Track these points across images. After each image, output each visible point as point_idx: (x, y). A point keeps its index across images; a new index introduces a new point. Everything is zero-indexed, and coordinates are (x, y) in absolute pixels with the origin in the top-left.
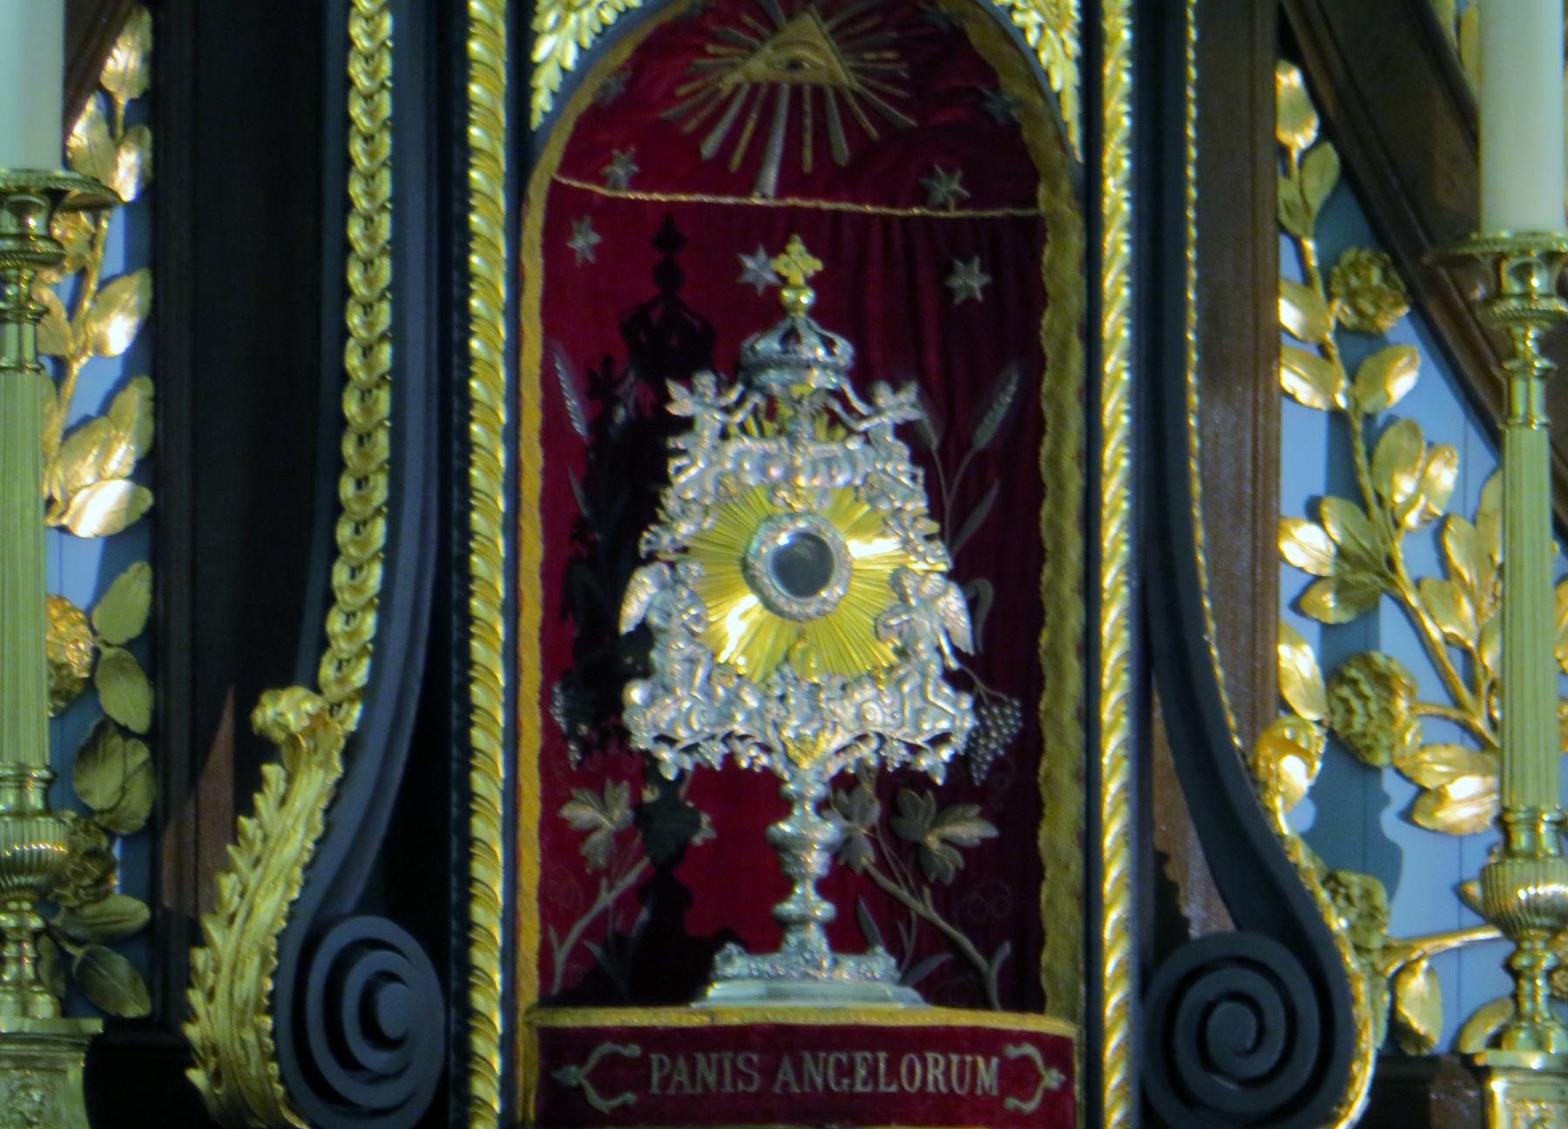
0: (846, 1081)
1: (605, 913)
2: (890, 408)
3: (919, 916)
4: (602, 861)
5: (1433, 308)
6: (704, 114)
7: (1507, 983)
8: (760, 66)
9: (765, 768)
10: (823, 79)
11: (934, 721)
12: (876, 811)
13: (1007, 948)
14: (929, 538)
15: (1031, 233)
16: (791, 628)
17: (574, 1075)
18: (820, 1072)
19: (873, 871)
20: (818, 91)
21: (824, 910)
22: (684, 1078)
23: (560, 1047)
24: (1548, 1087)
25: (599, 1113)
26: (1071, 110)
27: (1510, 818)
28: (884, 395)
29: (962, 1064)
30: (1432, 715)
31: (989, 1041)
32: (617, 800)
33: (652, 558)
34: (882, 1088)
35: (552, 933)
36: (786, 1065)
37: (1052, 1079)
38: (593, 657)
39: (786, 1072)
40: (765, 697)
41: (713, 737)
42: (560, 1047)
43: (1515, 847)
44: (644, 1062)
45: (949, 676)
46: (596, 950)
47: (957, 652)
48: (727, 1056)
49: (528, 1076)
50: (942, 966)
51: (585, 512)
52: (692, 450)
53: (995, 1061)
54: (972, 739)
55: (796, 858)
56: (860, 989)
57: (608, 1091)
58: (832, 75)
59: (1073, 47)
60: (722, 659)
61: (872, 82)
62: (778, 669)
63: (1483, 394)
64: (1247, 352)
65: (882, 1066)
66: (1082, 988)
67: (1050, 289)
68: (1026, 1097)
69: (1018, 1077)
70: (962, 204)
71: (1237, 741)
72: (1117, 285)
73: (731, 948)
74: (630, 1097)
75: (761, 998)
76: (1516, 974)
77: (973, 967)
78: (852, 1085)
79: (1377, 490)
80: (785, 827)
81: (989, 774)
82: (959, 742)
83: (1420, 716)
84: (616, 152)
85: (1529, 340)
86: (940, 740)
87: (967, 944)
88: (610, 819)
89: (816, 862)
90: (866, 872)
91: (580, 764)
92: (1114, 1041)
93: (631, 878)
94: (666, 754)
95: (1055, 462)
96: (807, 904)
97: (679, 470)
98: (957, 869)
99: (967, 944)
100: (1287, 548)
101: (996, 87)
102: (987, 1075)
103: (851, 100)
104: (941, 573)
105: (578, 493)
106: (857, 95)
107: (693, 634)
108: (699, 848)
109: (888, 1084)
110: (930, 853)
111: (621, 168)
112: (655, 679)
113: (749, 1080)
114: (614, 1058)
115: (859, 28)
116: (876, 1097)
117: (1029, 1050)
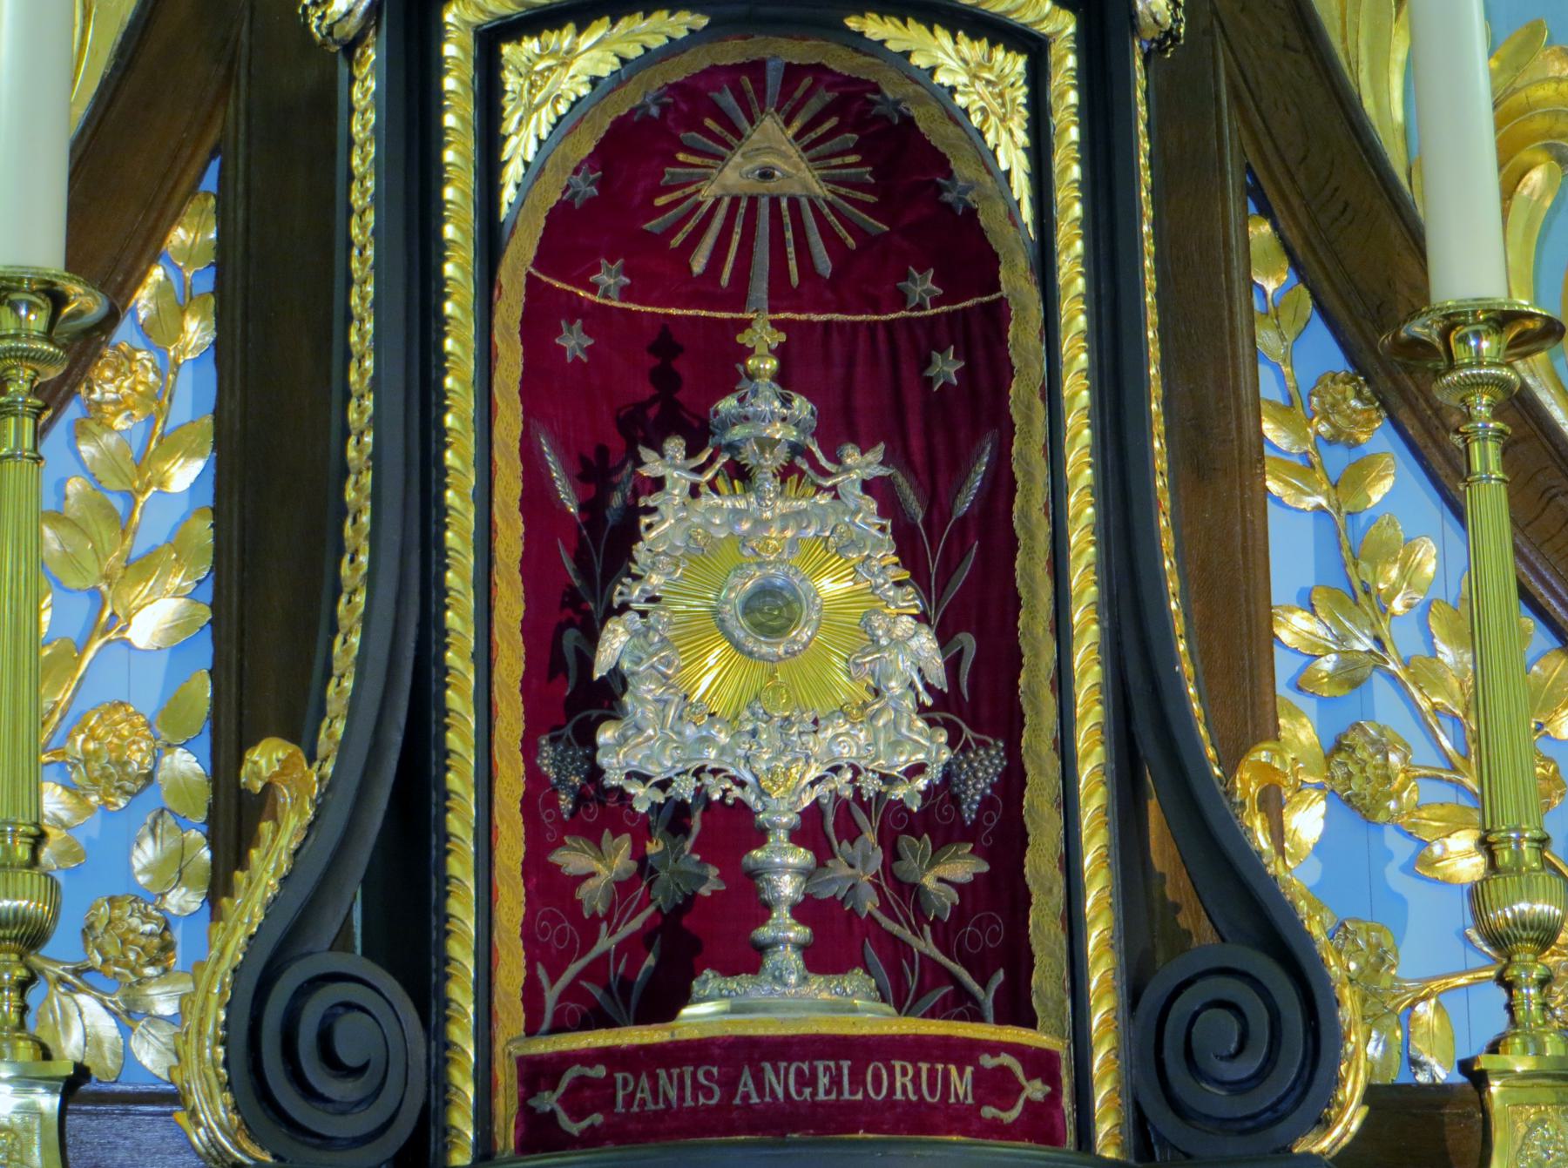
0: (807, 1091)
1: (605, 956)
2: (859, 467)
3: (921, 954)
4: (601, 909)
5: (1403, 414)
6: (689, 227)
7: (1502, 994)
8: (733, 176)
9: (738, 800)
10: (797, 190)
11: (906, 751)
12: (878, 856)
13: (1000, 976)
14: (899, 584)
15: (997, 315)
16: (758, 672)
17: (548, 1101)
18: (780, 1082)
19: (878, 915)
20: (794, 203)
21: (799, 932)
22: (647, 1095)
23: (536, 1073)
24: (1545, 1091)
25: (569, 1135)
26: (1021, 187)
27: (1492, 838)
28: (851, 455)
29: (932, 1074)
30: (1426, 777)
31: (964, 1051)
32: (617, 849)
33: (625, 607)
34: (846, 1096)
35: (541, 972)
36: (746, 1076)
37: (1036, 1090)
38: (573, 699)
39: (747, 1082)
40: (738, 733)
41: (686, 772)
42: (536, 1073)
43: (1500, 863)
44: (609, 1081)
45: (922, 709)
46: (597, 992)
47: (929, 688)
48: (688, 1070)
49: (506, 1106)
50: (945, 997)
51: (577, 583)
52: (663, 508)
53: (969, 1070)
54: (947, 775)
55: (769, 881)
56: (853, 1006)
57: (577, 1114)
58: (805, 186)
59: (1022, 138)
60: (695, 698)
61: (843, 191)
62: (749, 707)
63: (1443, 471)
64: (1221, 461)
65: (846, 1072)
66: (1068, 1004)
67: (1015, 361)
68: (1008, 1107)
69: (997, 1086)
70: (936, 302)
71: (1217, 771)
72: (1077, 358)
73: (708, 973)
74: (597, 1118)
75: (724, 1013)
76: (1509, 986)
77: (971, 997)
78: (814, 1094)
79: (1364, 561)
80: (758, 854)
81: (978, 813)
82: (935, 773)
83: (1415, 777)
84: (603, 262)
85: (1482, 404)
86: (916, 770)
87: (965, 976)
88: (610, 869)
89: (787, 887)
90: (870, 915)
91: (573, 814)
92: (1101, 1055)
93: (636, 924)
94: (636, 789)
95: (1025, 515)
96: (785, 932)
97: (649, 527)
98: (953, 904)
99: (965, 976)
100: (1284, 635)
101: (949, 174)
102: (961, 1084)
103: (826, 210)
104: (914, 616)
105: (569, 565)
106: (830, 205)
107: (666, 677)
108: (706, 898)
109: (853, 1092)
110: (927, 893)
111: (609, 279)
112: (626, 720)
113: (709, 1094)
114: (582, 1081)
115: (820, 131)
116: (841, 1108)
117: (1006, 1059)
